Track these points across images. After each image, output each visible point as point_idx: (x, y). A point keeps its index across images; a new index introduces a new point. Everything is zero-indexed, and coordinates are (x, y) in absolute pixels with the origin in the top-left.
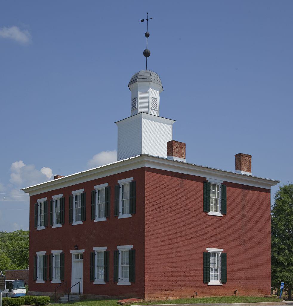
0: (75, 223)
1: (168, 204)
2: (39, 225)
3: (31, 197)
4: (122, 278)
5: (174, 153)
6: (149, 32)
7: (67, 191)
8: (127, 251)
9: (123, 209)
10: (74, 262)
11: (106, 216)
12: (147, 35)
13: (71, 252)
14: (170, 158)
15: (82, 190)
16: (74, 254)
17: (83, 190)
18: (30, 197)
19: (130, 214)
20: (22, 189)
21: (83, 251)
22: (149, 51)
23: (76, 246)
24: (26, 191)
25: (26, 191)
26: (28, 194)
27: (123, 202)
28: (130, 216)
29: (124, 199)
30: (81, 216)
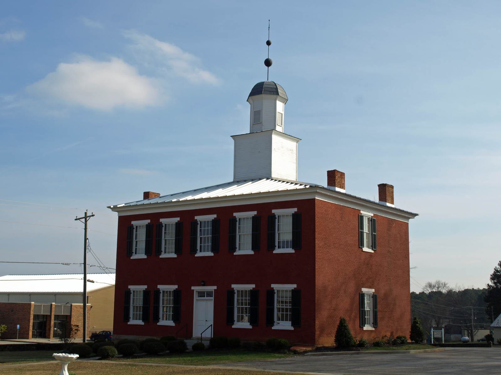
0: (365, 249)
1: (333, 239)
2: (134, 253)
3: (120, 218)
4: (279, 322)
5: (336, 183)
6: (271, 40)
7: (155, 218)
8: (290, 291)
9: (136, 249)
10: (197, 300)
11: (146, 253)
12: (268, 43)
13: (193, 288)
14: (331, 188)
15: (178, 219)
16: (196, 290)
17: (178, 219)
18: (119, 217)
19: (252, 250)
20: (109, 207)
21: (215, 287)
22: (272, 61)
23: (203, 282)
24: (115, 209)
25: (115, 209)
26: (117, 213)
27: (279, 234)
28: (175, 256)
29: (138, 239)
30: (211, 245)
